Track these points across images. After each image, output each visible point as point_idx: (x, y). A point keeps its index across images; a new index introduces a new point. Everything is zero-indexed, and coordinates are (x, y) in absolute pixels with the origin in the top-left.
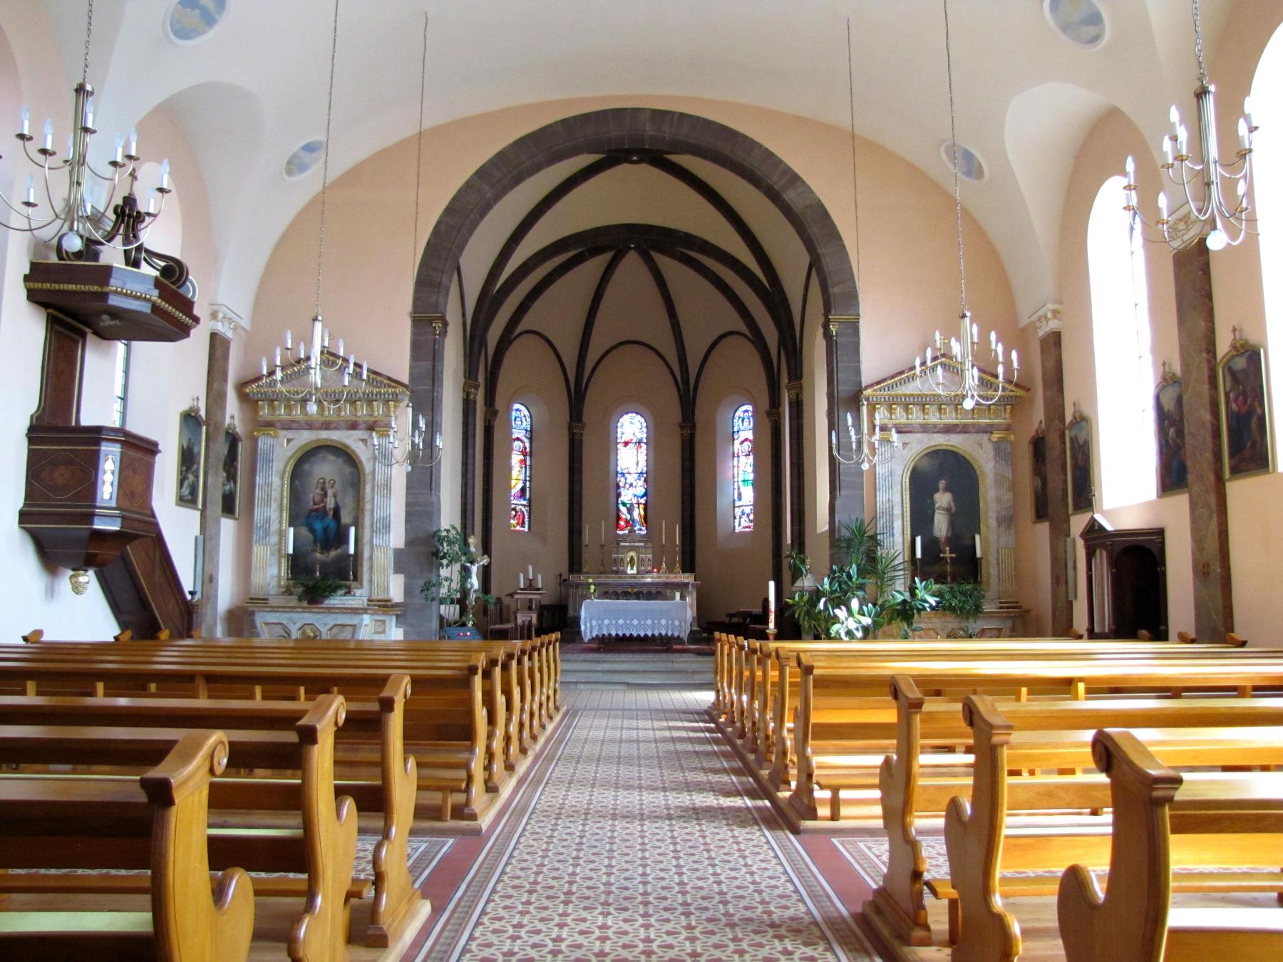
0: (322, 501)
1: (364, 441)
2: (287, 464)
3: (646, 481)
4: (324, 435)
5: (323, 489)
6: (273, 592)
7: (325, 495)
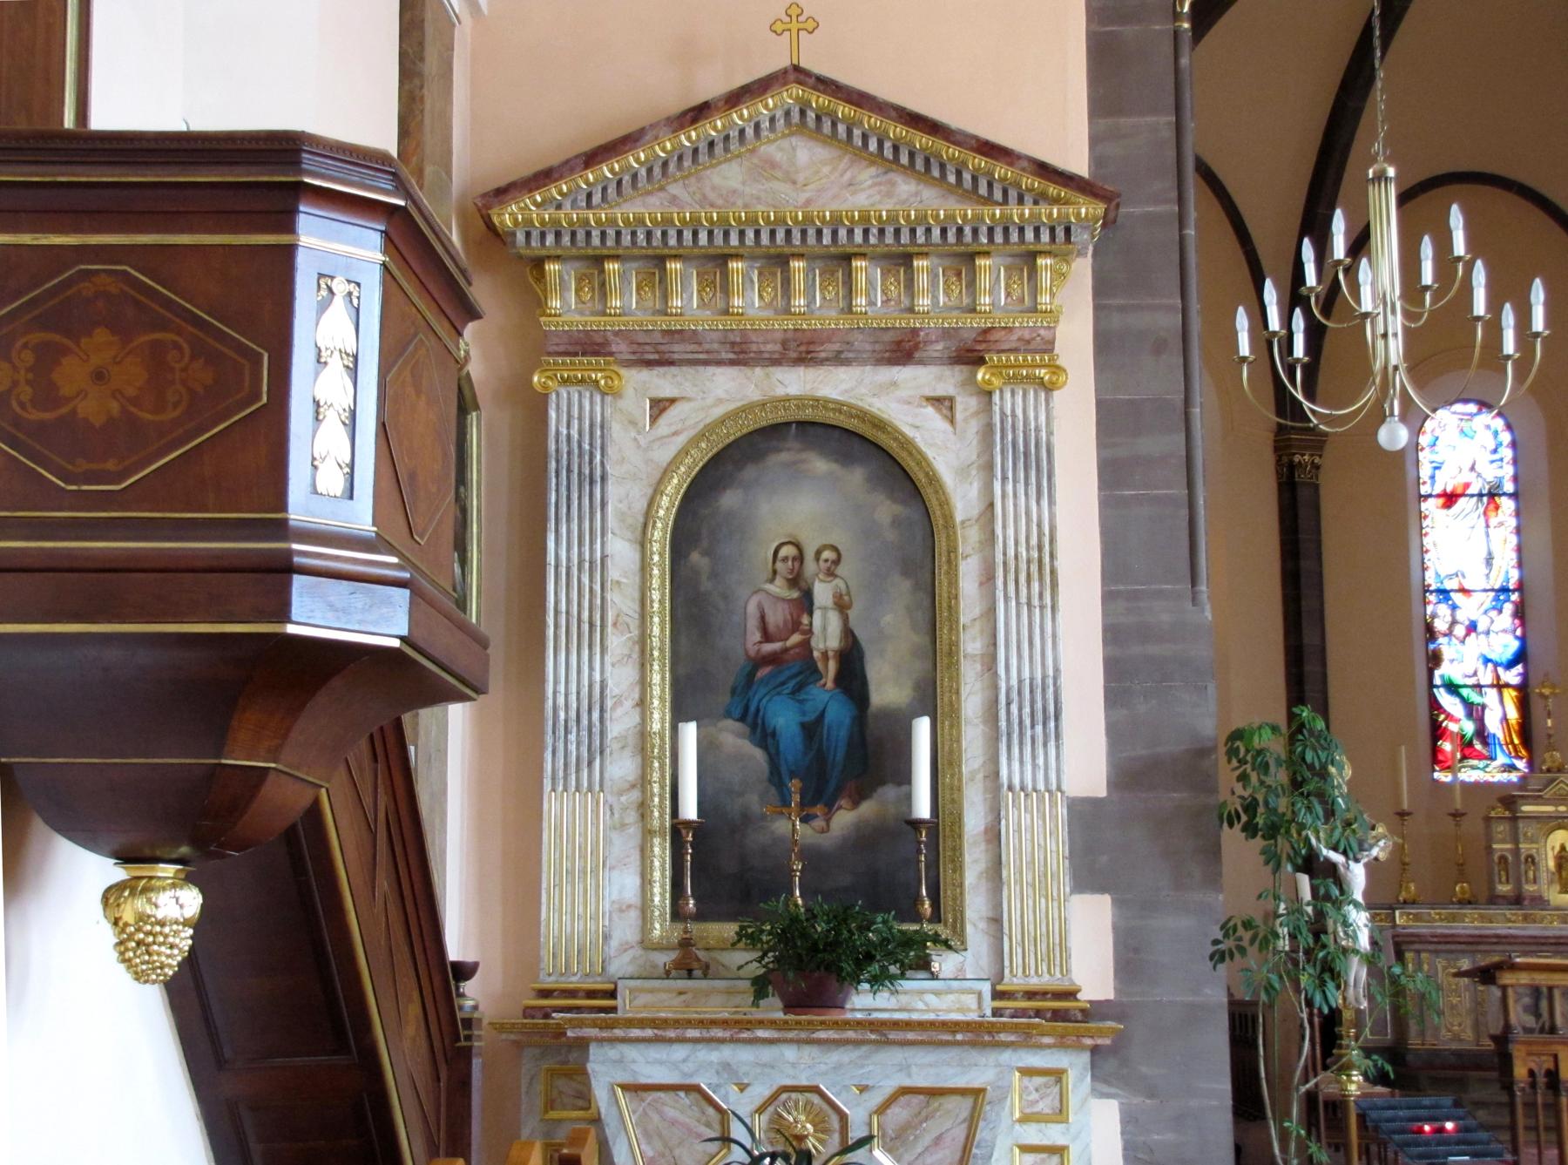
0: (795, 626)
1: (943, 403)
2: (657, 491)
3: (1520, 613)
4: (794, 383)
5: (795, 581)
6: (621, 965)
7: (806, 602)
